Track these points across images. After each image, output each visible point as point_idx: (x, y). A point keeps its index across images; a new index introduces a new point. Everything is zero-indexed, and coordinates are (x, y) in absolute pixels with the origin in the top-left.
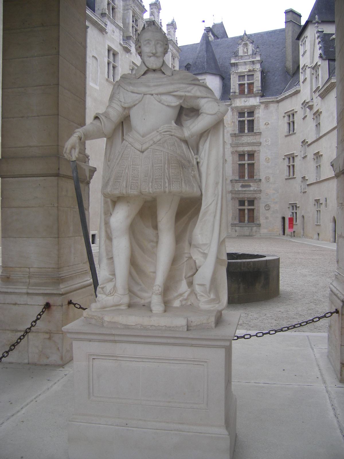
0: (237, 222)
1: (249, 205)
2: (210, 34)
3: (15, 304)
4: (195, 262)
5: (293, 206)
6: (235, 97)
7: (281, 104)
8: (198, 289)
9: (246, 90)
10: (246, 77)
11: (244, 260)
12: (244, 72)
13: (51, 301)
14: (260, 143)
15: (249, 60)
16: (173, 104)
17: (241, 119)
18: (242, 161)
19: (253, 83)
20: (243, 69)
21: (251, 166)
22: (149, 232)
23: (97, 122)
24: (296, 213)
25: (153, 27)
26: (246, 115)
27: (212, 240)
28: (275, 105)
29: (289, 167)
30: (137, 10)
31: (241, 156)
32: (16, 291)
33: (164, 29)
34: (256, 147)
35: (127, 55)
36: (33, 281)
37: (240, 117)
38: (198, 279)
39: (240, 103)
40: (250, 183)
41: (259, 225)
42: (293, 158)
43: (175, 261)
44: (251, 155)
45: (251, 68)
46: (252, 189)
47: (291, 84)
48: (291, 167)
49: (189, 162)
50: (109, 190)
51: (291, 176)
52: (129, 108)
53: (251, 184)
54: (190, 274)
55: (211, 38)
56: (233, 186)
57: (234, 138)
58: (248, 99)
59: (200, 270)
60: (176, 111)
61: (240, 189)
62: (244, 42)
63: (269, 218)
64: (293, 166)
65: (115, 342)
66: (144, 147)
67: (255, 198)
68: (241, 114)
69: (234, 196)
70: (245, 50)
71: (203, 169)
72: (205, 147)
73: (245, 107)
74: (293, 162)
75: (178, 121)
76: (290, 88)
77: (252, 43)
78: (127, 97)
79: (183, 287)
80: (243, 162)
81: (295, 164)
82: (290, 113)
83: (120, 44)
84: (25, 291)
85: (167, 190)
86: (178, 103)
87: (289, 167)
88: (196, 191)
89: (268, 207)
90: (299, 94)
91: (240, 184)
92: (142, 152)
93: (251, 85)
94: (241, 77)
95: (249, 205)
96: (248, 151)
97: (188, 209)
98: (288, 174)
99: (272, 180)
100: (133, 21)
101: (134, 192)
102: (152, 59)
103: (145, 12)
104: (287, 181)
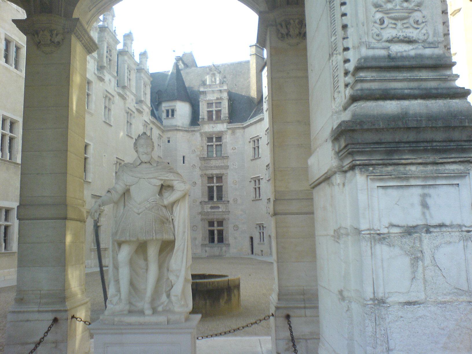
0: (207, 242)
1: (218, 226)
2: (181, 63)
3: (27, 321)
4: (171, 282)
5: (260, 227)
6: (204, 123)
7: (246, 130)
8: (173, 298)
9: (214, 117)
10: (214, 105)
11: (201, 281)
12: (212, 100)
13: (59, 316)
14: (228, 167)
15: (217, 89)
16: (157, 184)
17: (210, 144)
18: (211, 183)
19: (220, 111)
20: (212, 97)
21: (220, 189)
22: (141, 262)
23: (109, 194)
24: (263, 233)
25: (145, 136)
26: (214, 140)
27: (181, 268)
28: (241, 131)
29: (255, 189)
30: (111, 41)
31: (210, 178)
32: (29, 310)
33: (137, 59)
34: (224, 170)
35: (101, 84)
36: (43, 301)
37: (209, 142)
38: (173, 292)
39: (209, 128)
40: (266, 115)
41: (228, 245)
42: (259, 180)
43: (159, 280)
44: (220, 178)
45: (219, 97)
46: (220, 210)
47: (255, 111)
48: (257, 189)
49: (167, 220)
50: (117, 238)
51: (258, 198)
52: (130, 186)
53: (220, 206)
54: (169, 289)
55: (181, 66)
56: (203, 208)
57: (203, 162)
58: (216, 125)
59: (174, 288)
60: (159, 188)
61: (209, 210)
62: (211, 73)
63: (236, 240)
64: (259, 188)
65: (122, 334)
66: (140, 211)
67: (224, 219)
68: (210, 139)
69: (203, 217)
70: (213, 80)
71: (176, 224)
72: (177, 210)
73: (214, 133)
74: (259, 184)
75: (160, 193)
76: (255, 115)
77: (220, 73)
78: (127, 178)
79: (164, 298)
80: (212, 185)
81: (261, 186)
82: (255, 139)
83: (95, 73)
84: (36, 309)
85: (154, 238)
86: (160, 184)
87: (255, 189)
88: (171, 237)
89: (236, 228)
90: (263, 122)
91: (210, 206)
92: (139, 214)
93: (218, 112)
94: (210, 104)
95: (218, 226)
96: (217, 174)
97: (167, 247)
98: (254, 197)
99: (239, 201)
100: (107, 52)
101: (135, 239)
102: (144, 156)
103: (118, 44)
104: (254, 202)
